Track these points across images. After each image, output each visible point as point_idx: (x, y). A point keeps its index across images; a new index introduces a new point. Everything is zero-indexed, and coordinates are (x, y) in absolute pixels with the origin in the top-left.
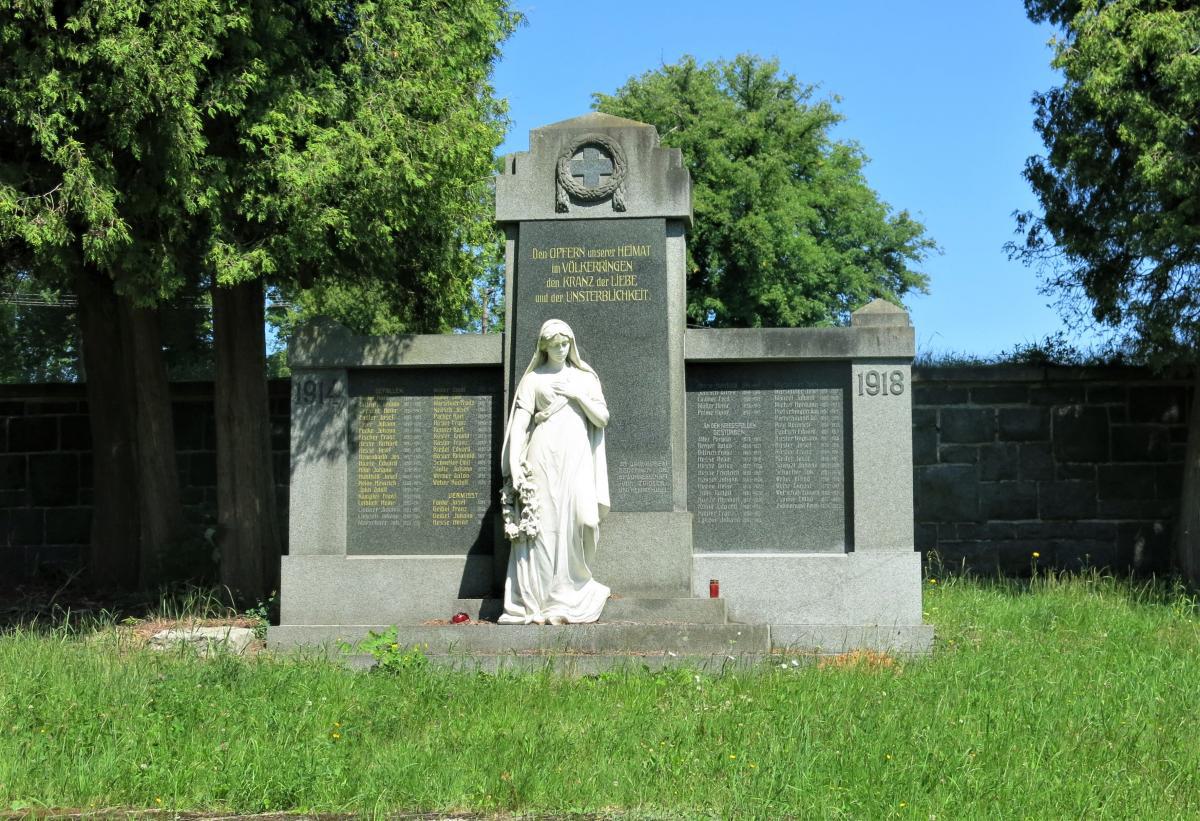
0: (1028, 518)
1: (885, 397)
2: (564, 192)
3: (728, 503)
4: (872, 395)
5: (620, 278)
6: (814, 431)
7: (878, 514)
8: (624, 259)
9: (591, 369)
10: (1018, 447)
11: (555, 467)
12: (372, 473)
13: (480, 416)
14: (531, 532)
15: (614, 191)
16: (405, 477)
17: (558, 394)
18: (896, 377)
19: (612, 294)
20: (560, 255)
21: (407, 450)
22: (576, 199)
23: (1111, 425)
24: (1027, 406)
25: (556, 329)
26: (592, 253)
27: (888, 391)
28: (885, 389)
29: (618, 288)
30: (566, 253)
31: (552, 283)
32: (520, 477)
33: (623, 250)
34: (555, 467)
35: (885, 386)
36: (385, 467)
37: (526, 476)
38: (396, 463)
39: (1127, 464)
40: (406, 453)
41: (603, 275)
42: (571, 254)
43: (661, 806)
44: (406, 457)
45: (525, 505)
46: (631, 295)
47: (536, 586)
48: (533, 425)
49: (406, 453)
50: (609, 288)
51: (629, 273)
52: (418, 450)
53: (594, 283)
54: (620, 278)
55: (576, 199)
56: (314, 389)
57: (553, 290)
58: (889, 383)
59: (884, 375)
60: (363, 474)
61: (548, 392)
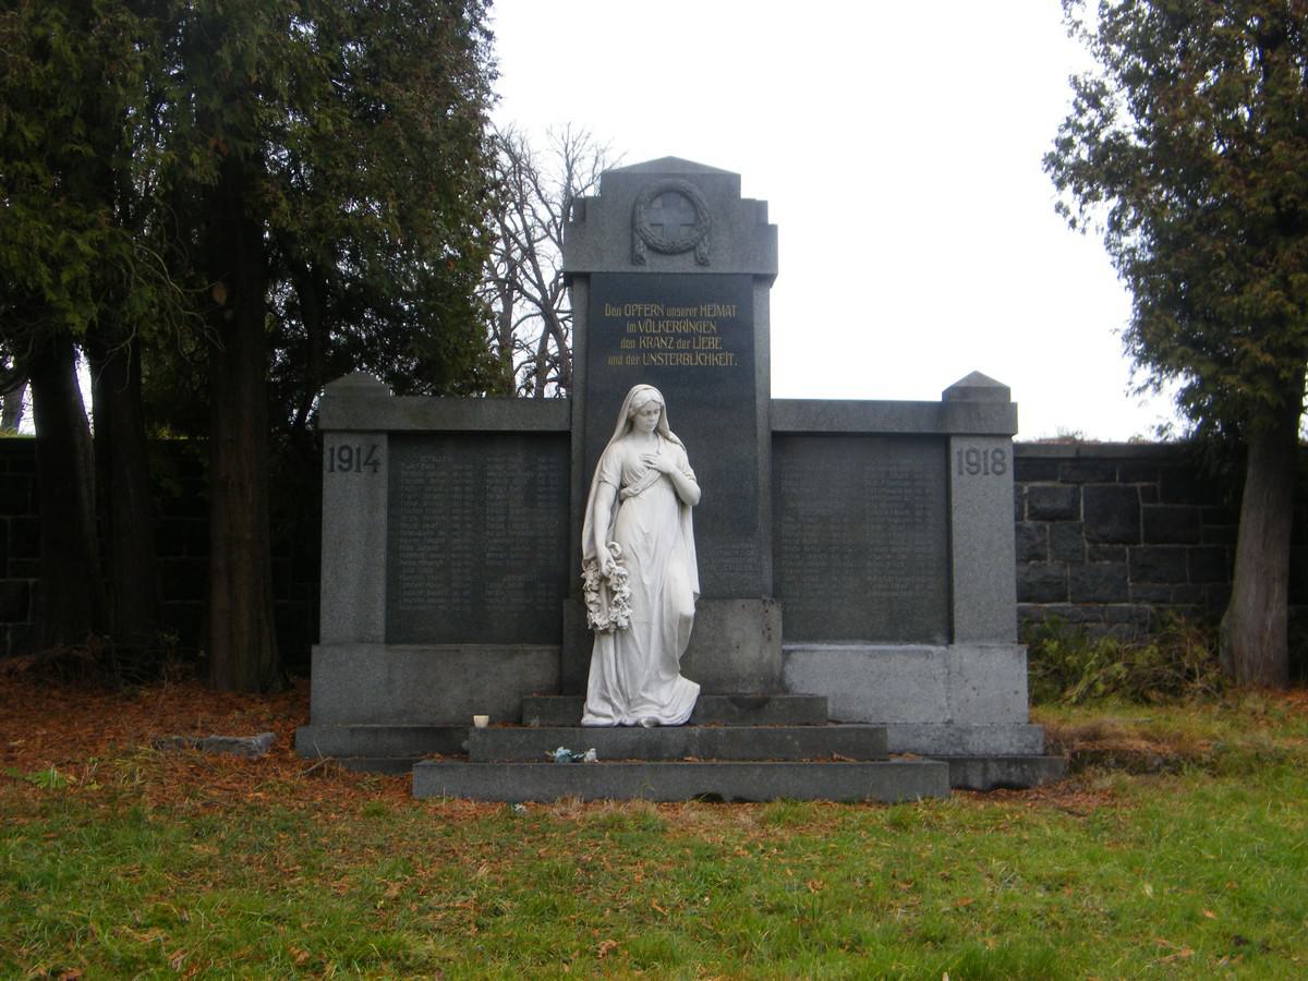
0: (1059, 601)
1: (986, 477)
2: (641, 243)
3: (815, 590)
4: (972, 474)
5: (702, 340)
6: (907, 512)
7: (979, 603)
8: (709, 319)
9: (679, 441)
10: (1048, 527)
11: (647, 550)
12: (415, 551)
13: (540, 489)
14: (623, 623)
15: (698, 244)
16: (453, 556)
17: (649, 468)
18: (998, 456)
19: (694, 357)
20: (636, 312)
21: (457, 526)
22: (654, 249)
23: (1142, 505)
24: (1056, 484)
25: (647, 395)
26: (672, 312)
27: (990, 471)
28: (986, 469)
29: (700, 351)
30: (642, 311)
31: (627, 344)
32: (609, 561)
33: (706, 310)
34: (647, 550)
35: (986, 465)
36: (431, 544)
37: (615, 559)
38: (443, 540)
39: (1159, 546)
40: (455, 530)
41: (684, 336)
42: (648, 312)
43: (433, 877)
44: (455, 533)
45: (616, 592)
46: (713, 360)
47: (623, 681)
48: (620, 499)
49: (455, 530)
50: (691, 350)
51: (713, 335)
52: (469, 526)
53: (674, 344)
54: (702, 340)
55: (654, 249)
56: (351, 456)
57: (627, 352)
58: (990, 462)
59: (985, 453)
60: (405, 552)
61: (638, 464)
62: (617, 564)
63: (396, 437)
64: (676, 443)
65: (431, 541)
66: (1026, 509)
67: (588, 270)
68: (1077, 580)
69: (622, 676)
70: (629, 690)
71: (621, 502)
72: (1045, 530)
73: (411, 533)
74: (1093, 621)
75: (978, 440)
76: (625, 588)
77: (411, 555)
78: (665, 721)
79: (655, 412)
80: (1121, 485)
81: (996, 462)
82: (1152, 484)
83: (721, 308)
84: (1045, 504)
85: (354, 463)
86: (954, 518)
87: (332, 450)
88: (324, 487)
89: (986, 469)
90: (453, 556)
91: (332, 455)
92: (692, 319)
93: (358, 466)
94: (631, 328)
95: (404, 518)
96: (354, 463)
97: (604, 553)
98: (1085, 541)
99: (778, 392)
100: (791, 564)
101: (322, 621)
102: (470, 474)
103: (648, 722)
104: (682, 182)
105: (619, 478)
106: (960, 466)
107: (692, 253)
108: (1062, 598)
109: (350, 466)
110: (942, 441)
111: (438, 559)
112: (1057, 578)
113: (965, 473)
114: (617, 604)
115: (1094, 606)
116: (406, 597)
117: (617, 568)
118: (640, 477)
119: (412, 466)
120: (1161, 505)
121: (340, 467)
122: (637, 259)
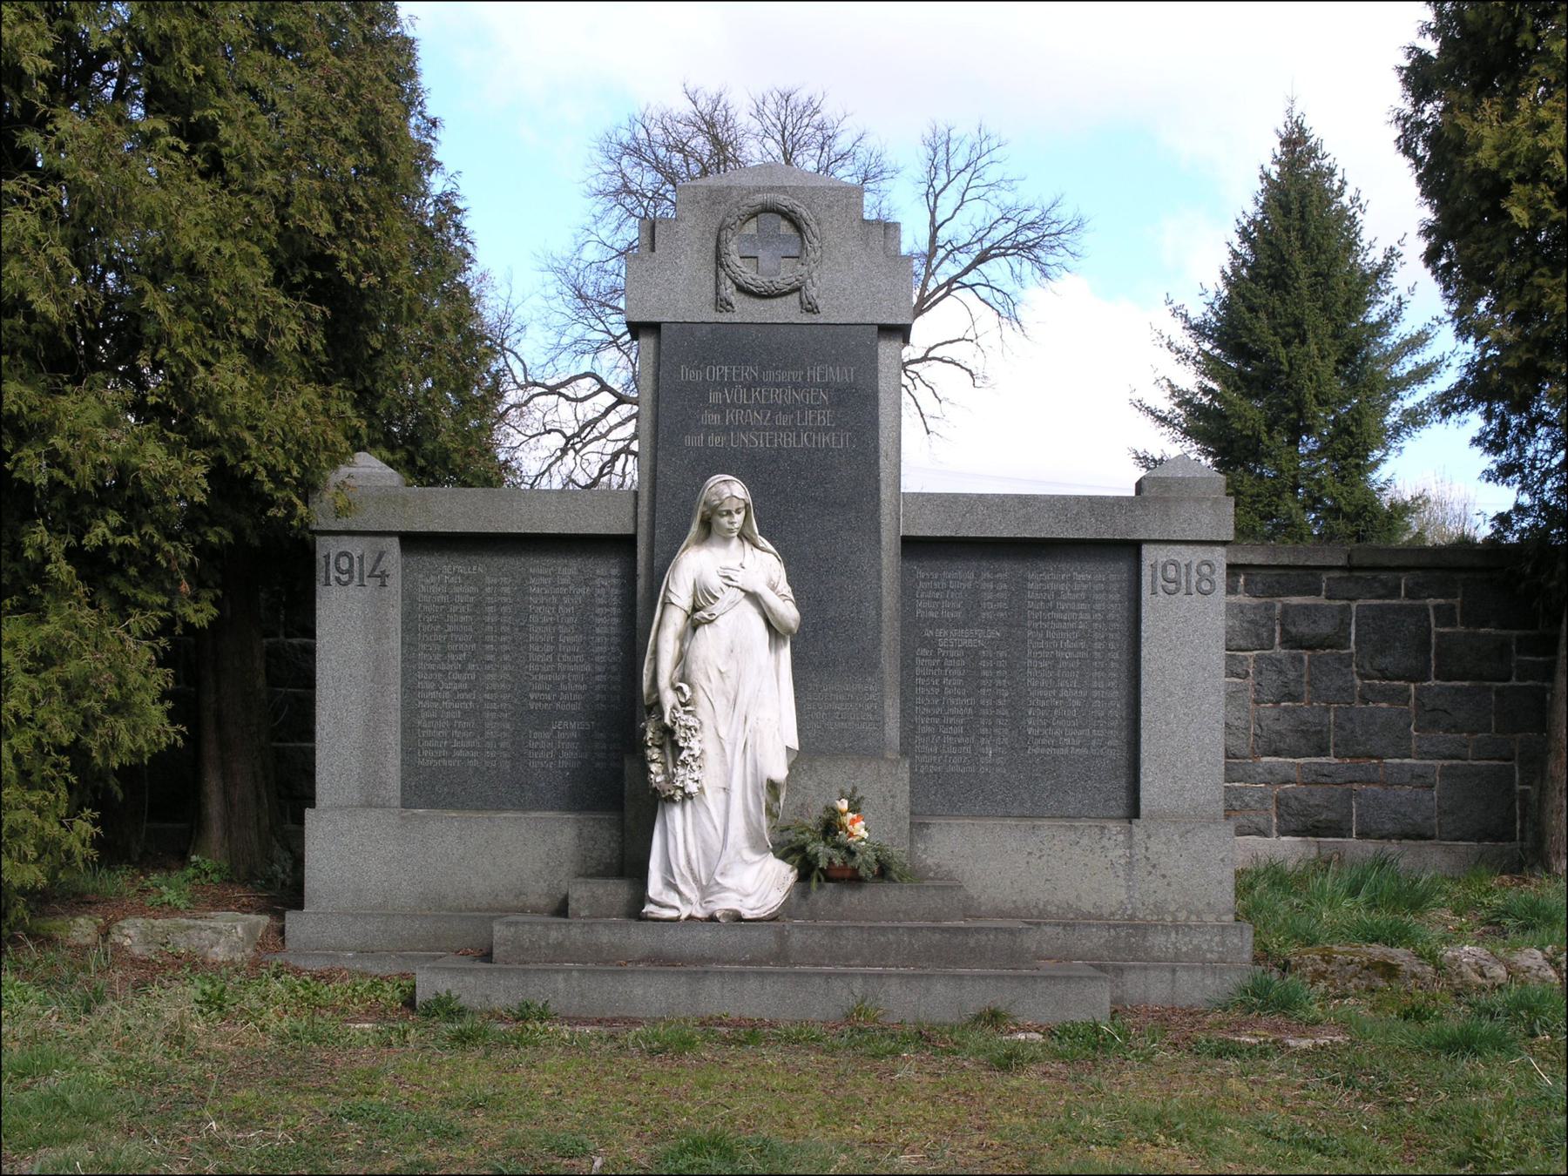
1: (1188, 598)
2: (729, 282)
5: (809, 414)
10: (1306, 658)
13: (598, 610)
19: (798, 436)
20: (722, 376)
21: (490, 657)
23: (1434, 629)
24: (1321, 600)
26: (769, 376)
27: (1194, 590)
28: (1188, 588)
29: (805, 429)
32: (674, 707)
35: (1188, 582)
36: (458, 681)
40: (489, 662)
41: (785, 409)
42: (738, 375)
44: (488, 667)
45: (683, 748)
51: (823, 406)
54: (809, 414)
56: (351, 565)
58: (1194, 577)
61: (715, 582)
62: (686, 712)
63: (413, 542)
64: (769, 552)
65: (458, 676)
66: (1277, 635)
67: (656, 319)
68: (1343, 729)
69: (693, 856)
70: (703, 875)
71: (695, 629)
72: (1301, 660)
73: (432, 667)
74: (1361, 782)
75: (1178, 548)
76: (694, 743)
77: (433, 695)
78: (748, 915)
79: (738, 512)
80: (1407, 602)
81: (1202, 577)
82: (1450, 601)
83: (835, 369)
84: (1303, 628)
85: (356, 574)
86: (1144, 652)
87: (327, 557)
88: (318, 606)
89: (1188, 588)
90: (487, 696)
91: (328, 564)
92: (796, 386)
93: (361, 579)
94: (714, 397)
95: (424, 646)
96: (356, 574)
97: (669, 698)
98: (1355, 676)
99: (914, 479)
100: (928, 710)
101: (318, 778)
102: (507, 590)
103: (724, 916)
104: (784, 200)
105: (691, 600)
106: (1153, 582)
107: (796, 295)
108: (1322, 751)
109: (352, 578)
110: (1132, 549)
111: (467, 701)
112: (1315, 725)
113: (1161, 593)
114: (684, 764)
115: (1364, 762)
116: (427, 748)
117: (684, 717)
118: (716, 598)
119: (433, 579)
120: (1461, 629)
121: (338, 579)
122: (722, 304)
